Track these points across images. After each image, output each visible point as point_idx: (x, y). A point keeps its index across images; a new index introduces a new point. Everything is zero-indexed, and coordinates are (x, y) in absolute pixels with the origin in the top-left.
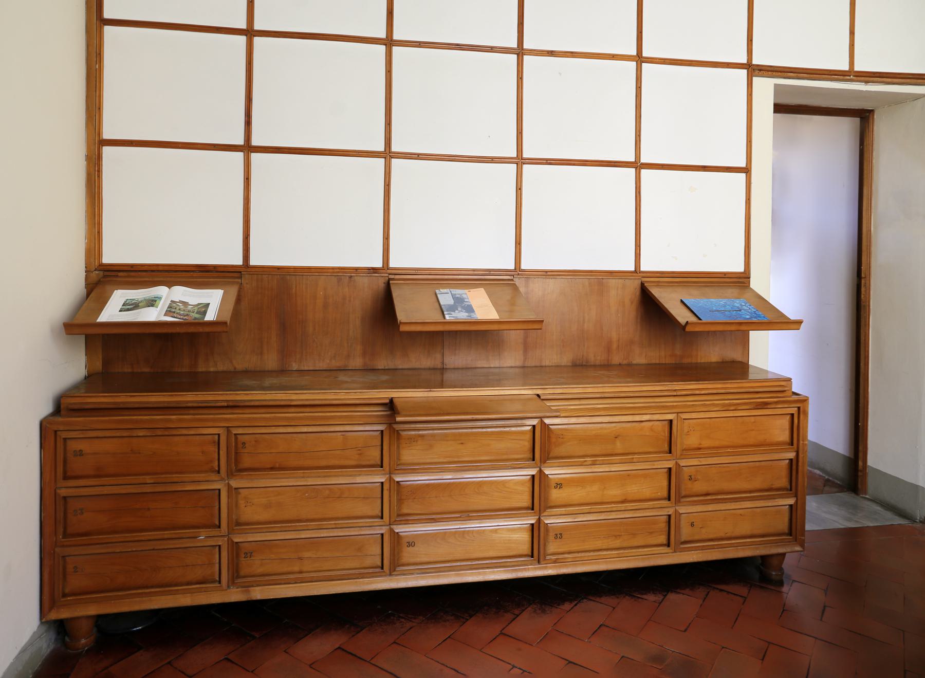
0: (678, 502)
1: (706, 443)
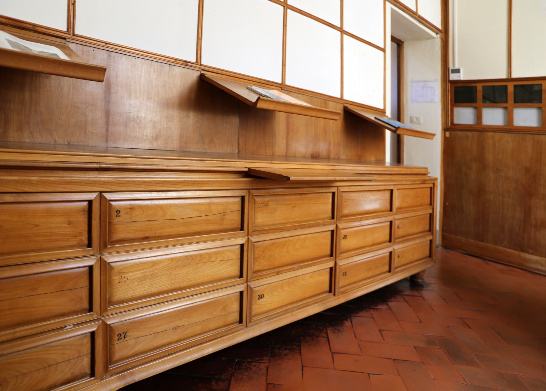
1: (404, 205)
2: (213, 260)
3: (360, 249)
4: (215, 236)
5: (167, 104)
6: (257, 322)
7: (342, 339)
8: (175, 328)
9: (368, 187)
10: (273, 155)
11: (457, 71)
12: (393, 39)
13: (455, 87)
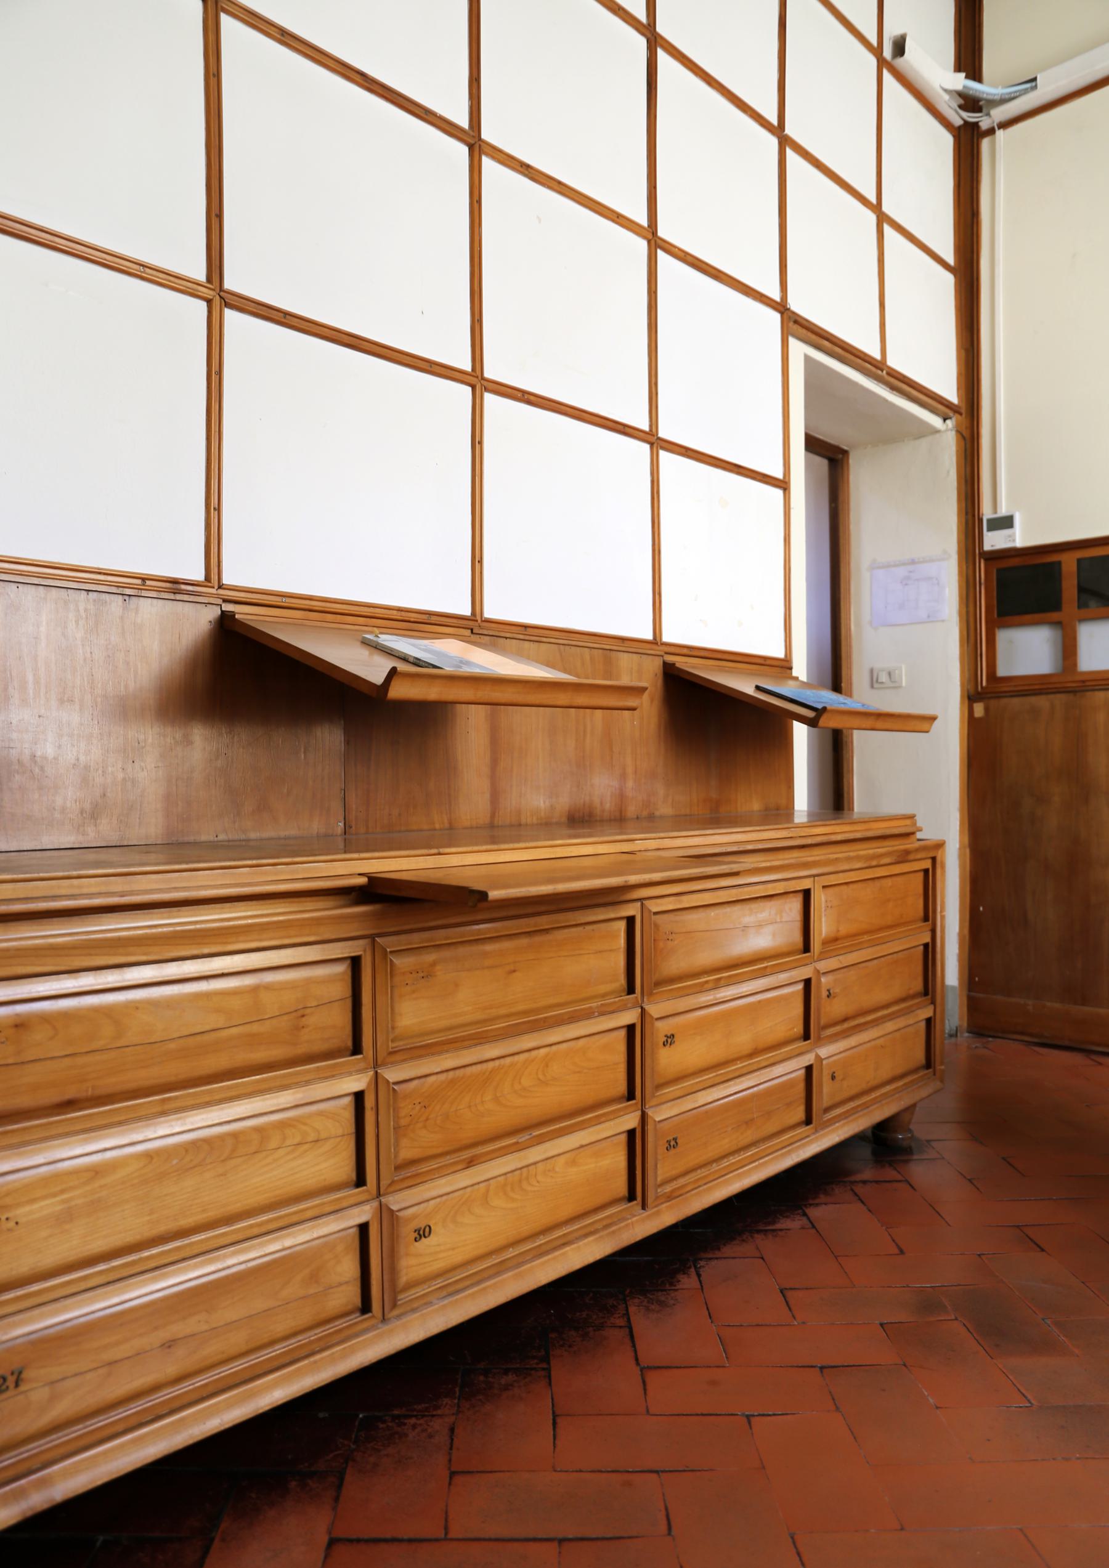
0: (820, 1041)
1: (844, 930)
2: (273, 1144)
3: (718, 1069)
4: (276, 1077)
5: (123, 710)
6: (415, 1305)
7: (668, 1329)
8: (169, 1345)
9: (734, 891)
10: (451, 828)
11: (1006, 522)
12: (813, 444)
13: (999, 571)
